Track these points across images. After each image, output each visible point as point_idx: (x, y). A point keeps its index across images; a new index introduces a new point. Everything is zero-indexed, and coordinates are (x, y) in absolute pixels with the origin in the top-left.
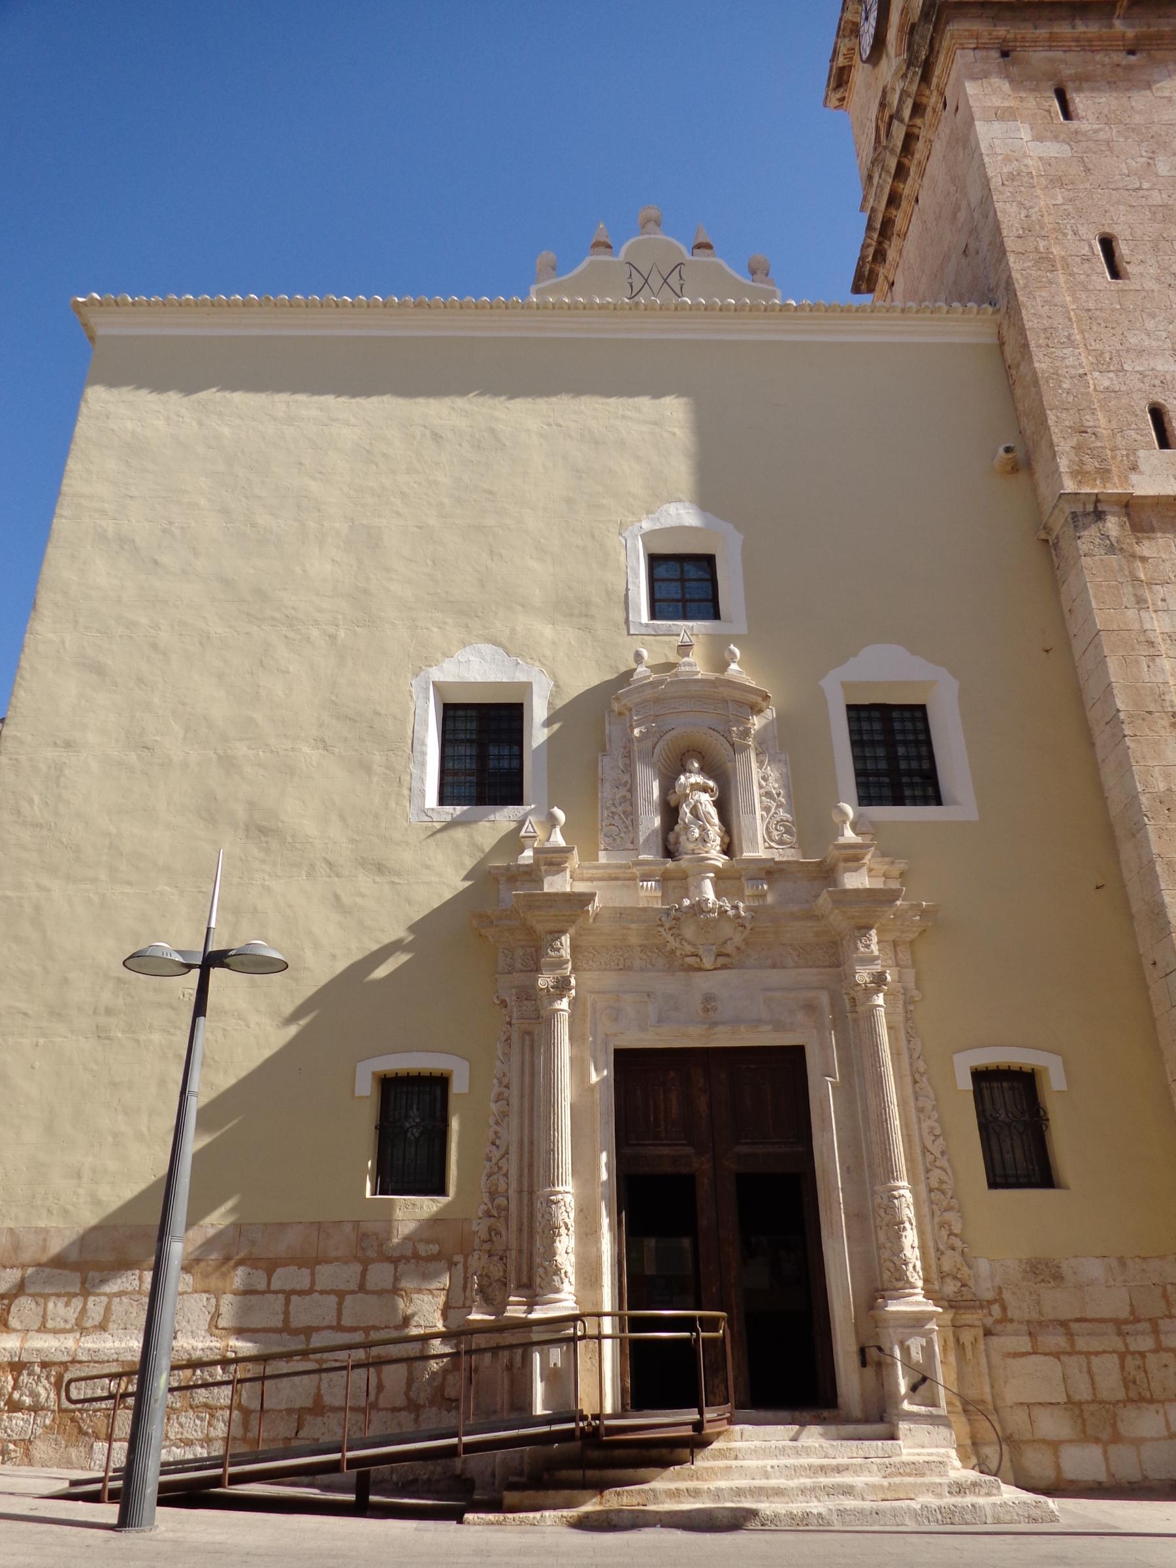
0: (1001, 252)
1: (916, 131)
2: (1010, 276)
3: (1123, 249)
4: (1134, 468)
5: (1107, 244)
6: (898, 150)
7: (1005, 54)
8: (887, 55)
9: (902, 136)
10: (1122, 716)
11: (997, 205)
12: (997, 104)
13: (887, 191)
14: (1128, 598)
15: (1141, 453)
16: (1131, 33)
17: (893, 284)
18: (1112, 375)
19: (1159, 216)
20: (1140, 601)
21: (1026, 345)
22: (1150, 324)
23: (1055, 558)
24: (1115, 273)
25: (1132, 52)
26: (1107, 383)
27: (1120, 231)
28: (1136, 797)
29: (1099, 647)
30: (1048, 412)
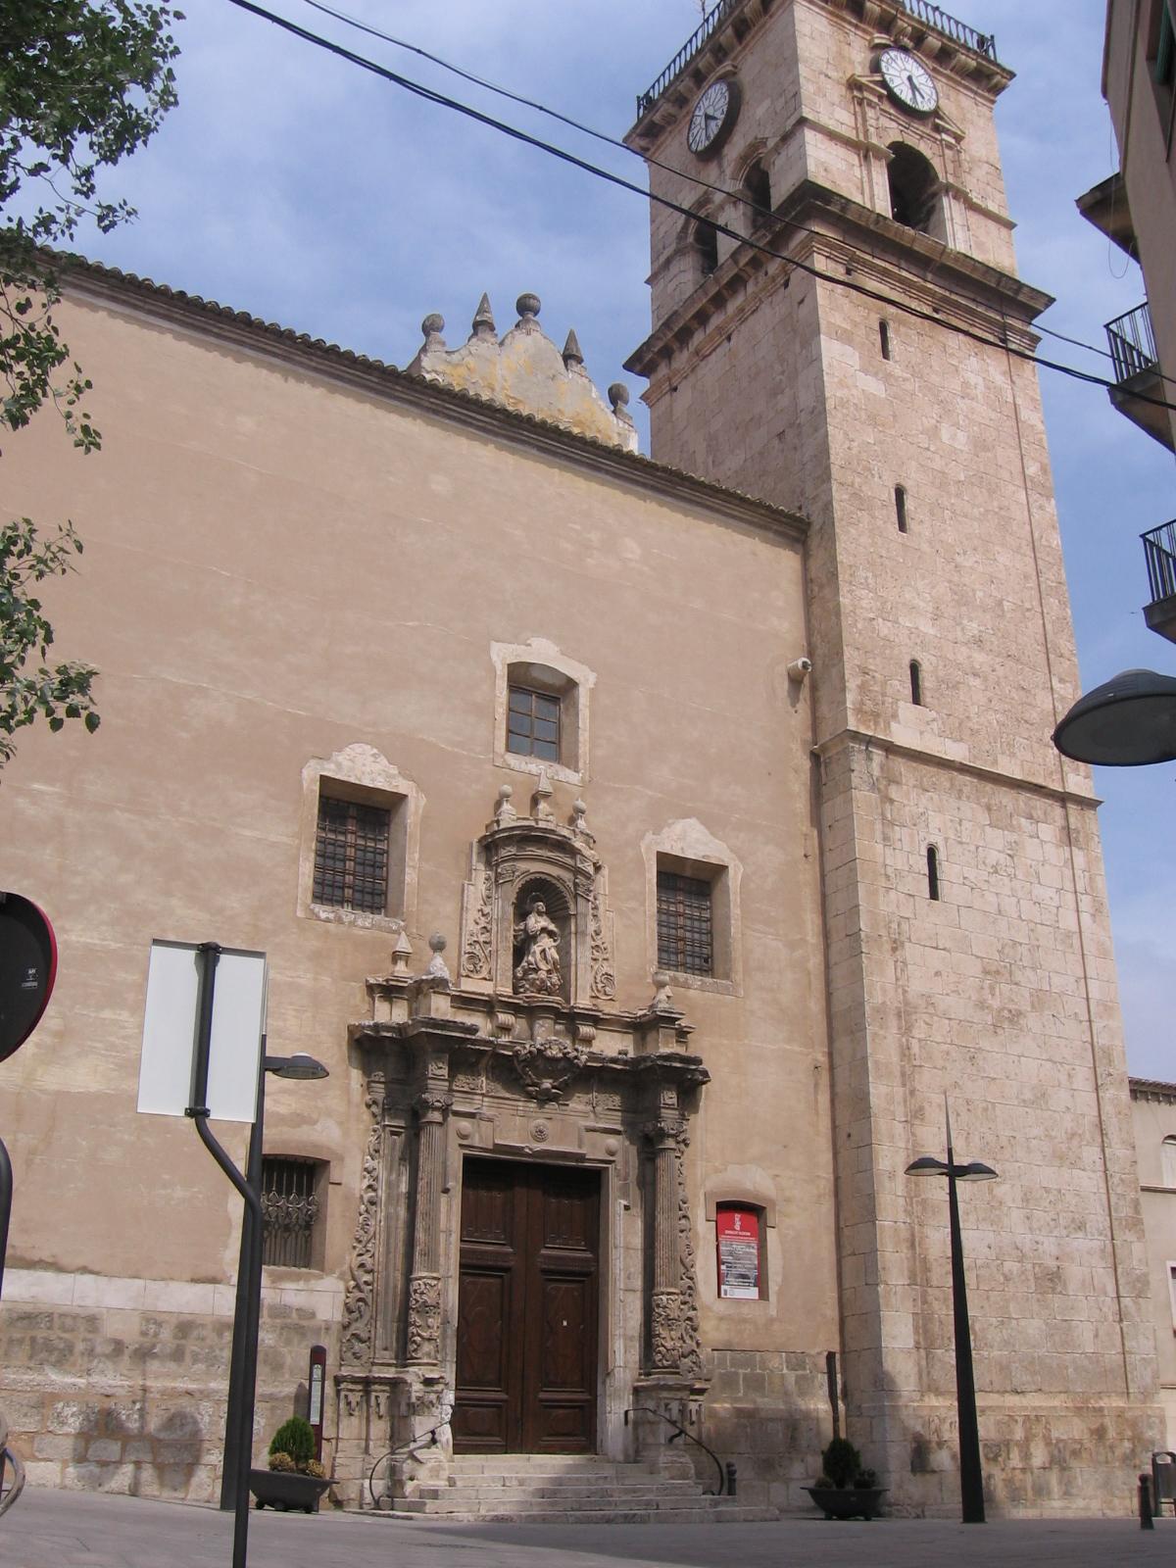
0: (825, 476)
1: (745, 276)
2: (830, 503)
3: (909, 504)
4: (895, 716)
5: (900, 493)
6: (725, 281)
8: (720, 165)
9: (731, 274)
10: (863, 934)
11: (830, 428)
12: (838, 323)
13: (698, 306)
14: (878, 836)
15: (901, 704)
17: (675, 389)
18: (889, 624)
19: (938, 481)
21: (834, 575)
22: (920, 584)
23: (824, 776)
24: (902, 527)
26: (886, 631)
27: (908, 485)
28: (862, 1004)
29: (854, 870)
30: (845, 648)
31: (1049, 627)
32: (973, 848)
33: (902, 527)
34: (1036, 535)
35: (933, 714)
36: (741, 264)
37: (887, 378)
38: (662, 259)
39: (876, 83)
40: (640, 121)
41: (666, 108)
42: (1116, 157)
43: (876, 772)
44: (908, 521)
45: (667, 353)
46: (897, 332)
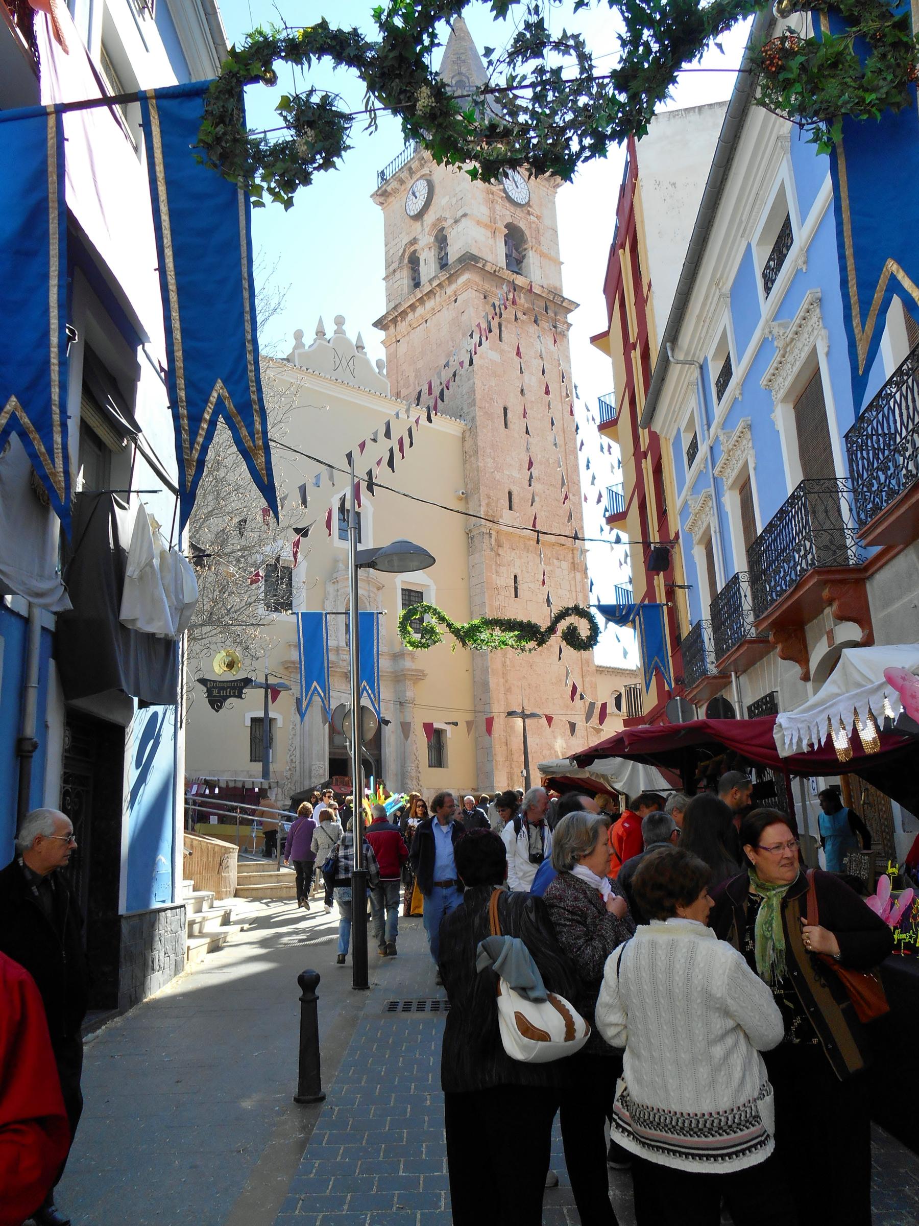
1: (435, 291)
5: (505, 409)
7: (485, 298)
13: (411, 302)
14: (494, 571)
15: (504, 510)
16: (526, 305)
17: (399, 341)
20: (497, 572)
24: (506, 426)
25: (524, 314)
27: (509, 405)
31: (569, 470)
32: (533, 574)
33: (506, 426)
34: (565, 425)
35: (518, 514)
36: (433, 286)
37: (502, 352)
38: (391, 269)
39: (500, 190)
40: (379, 188)
41: (394, 184)
42: (607, 325)
43: (493, 543)
44: (509, 423)
45: (394, 321)
46: (506, 328)
